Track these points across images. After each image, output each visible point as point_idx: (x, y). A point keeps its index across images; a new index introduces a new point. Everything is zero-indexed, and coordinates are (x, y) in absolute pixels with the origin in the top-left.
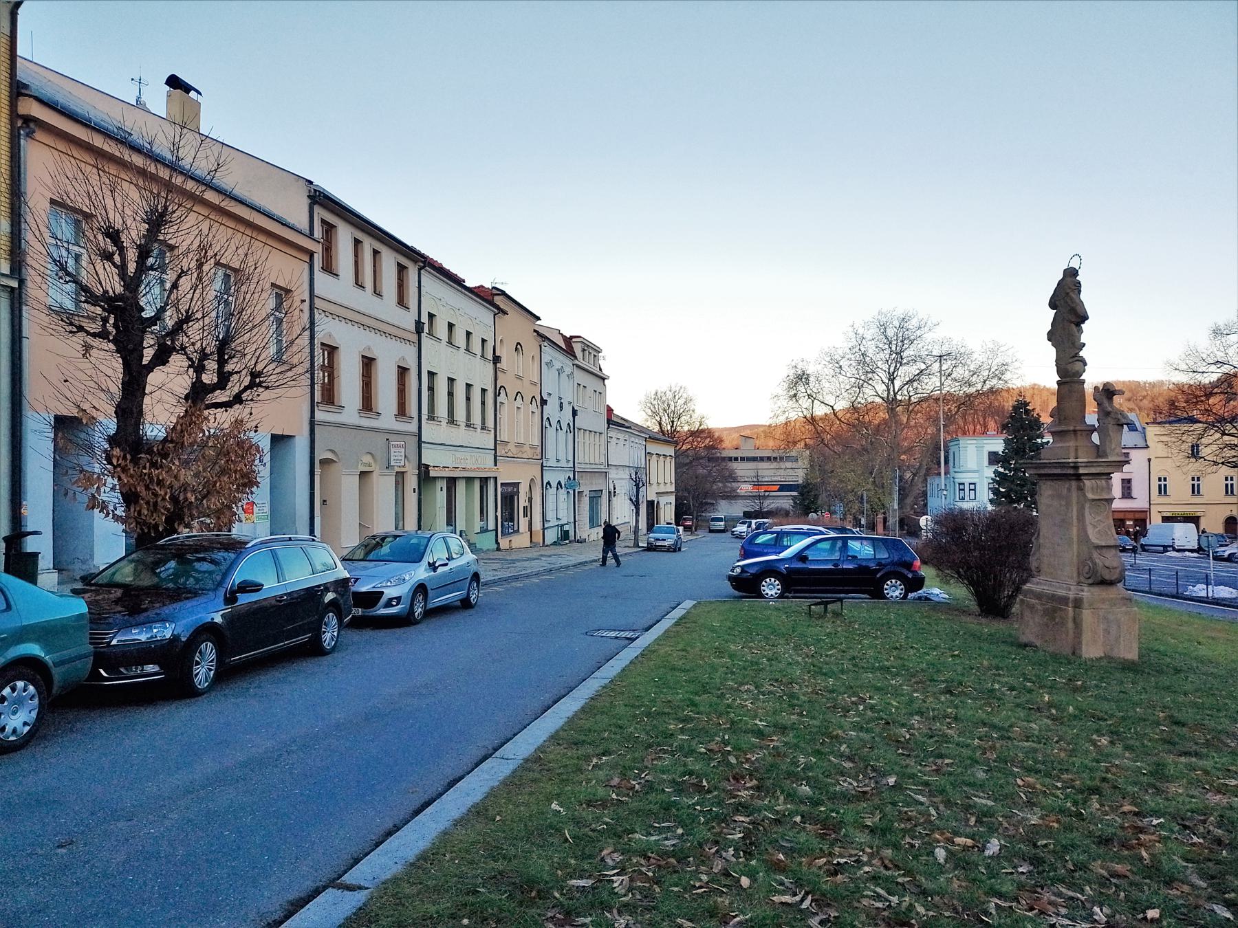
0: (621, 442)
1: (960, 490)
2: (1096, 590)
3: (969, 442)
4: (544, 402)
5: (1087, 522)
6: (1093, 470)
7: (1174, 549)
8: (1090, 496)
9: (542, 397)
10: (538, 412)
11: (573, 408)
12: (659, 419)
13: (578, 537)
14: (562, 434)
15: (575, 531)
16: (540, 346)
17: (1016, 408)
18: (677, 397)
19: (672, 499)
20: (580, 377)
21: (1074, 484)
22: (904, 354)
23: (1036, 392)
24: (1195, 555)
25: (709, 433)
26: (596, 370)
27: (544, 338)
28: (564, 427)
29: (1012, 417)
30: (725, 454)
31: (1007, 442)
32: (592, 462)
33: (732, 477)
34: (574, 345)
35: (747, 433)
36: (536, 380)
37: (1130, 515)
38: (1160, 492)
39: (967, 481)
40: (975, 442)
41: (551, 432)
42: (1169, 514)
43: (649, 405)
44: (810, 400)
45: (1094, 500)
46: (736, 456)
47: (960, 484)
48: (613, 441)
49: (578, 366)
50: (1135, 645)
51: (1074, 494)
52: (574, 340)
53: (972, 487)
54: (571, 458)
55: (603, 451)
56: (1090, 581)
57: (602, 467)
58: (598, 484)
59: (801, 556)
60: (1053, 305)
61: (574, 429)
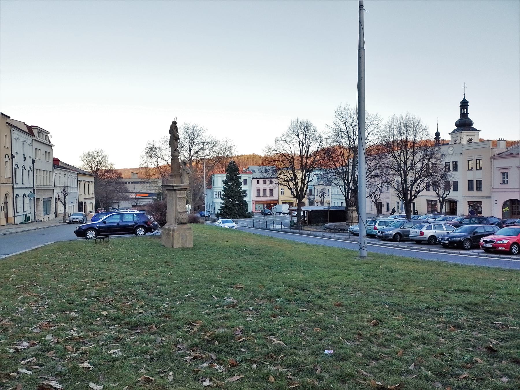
0: (62, 176)
1: (215, 194)
2: (180, 226)
3: (218, 176)
4: (13, 157)
5: (177, 205)
6: (179, 188)
7: (282, 214)
8: (178, 196)
9: (12, 155)
10: (10, 162)
11: (33, 160)
12: (90, 165)
13: (37, 219)
14: (26, 173)
15: (35, 217)
16: (11, 130)
17: (230, 163)
18: (99, 155)
19: (93, 201)
20: (36, 145)
21: (174, 192)
22: (195, 141)
23: (254, 157)
24: (288, 215)
25: (116, 171)
26: (49, 144)
27: (13, 126)
28: (27, 168)
29: (229, 167)
30: (123, 180)
31: (227, 176)
32: (45, 184)
33: (126, 190)
34: (33, 130)
35: (133, 172)
36: (8, 146)
37: (272, 202)
38: (281, 194)
39: (218, 191)
40: (248, 175)
41: (19, 172)
42: (284, 202)
43: (85, 158)
44: (156, 158)
45: (179, 197)
46: (129, 181)
47: (215, 192)
48: (58, 175)
49: (35, 140)
50: (192, 243)
51: (174, 195)
52: (33, 128)
53: (220, 193)
54: (32, 182)
55: (52, 180)
56: (178, 223)
57: (51, 187)
58: (48, 195)
59: (104, 222)
60: (170, 133)
61: (33, 169)
